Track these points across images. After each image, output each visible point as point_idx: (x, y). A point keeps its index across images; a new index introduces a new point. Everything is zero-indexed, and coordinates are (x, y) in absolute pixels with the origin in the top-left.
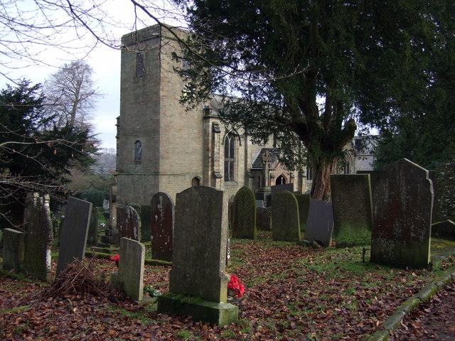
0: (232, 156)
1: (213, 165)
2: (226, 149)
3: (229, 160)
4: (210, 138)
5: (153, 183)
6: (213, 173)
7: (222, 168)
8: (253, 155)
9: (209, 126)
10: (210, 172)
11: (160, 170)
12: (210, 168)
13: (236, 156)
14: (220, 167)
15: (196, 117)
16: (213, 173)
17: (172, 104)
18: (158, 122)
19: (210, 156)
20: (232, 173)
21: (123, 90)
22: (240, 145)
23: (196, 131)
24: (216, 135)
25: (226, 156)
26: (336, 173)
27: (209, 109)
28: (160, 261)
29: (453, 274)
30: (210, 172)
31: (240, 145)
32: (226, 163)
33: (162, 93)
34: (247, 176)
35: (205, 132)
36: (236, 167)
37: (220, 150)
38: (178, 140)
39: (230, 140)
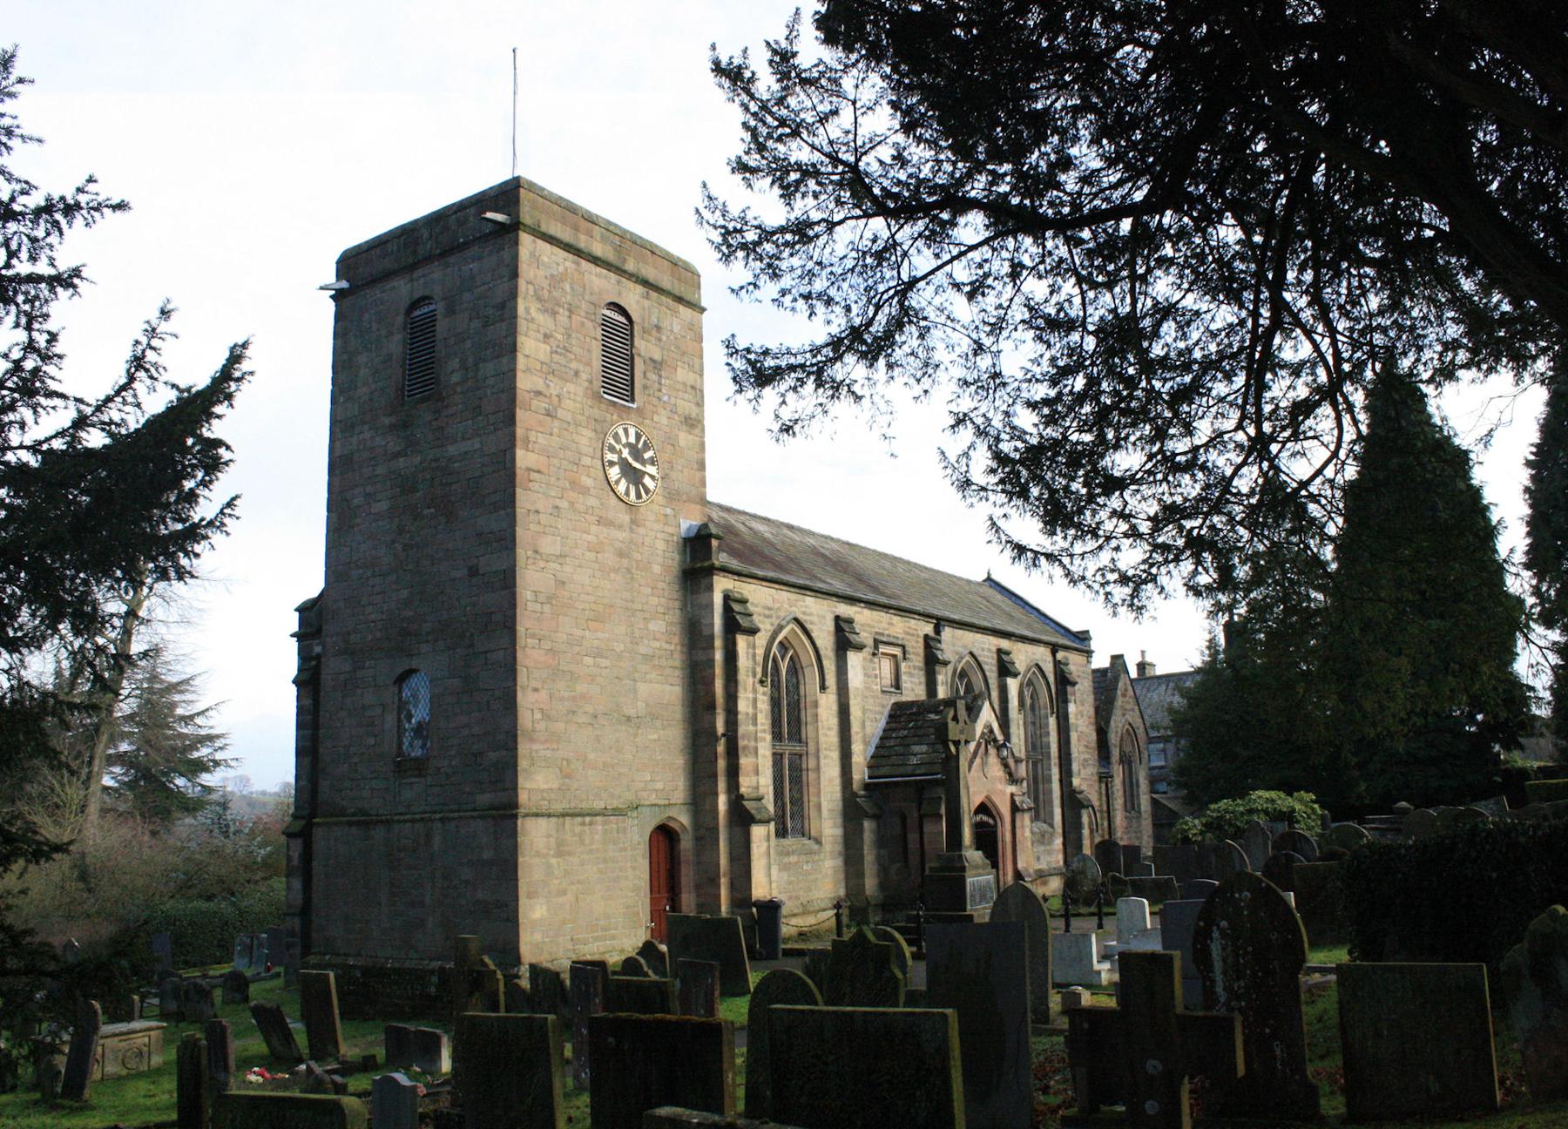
0: (796, 734)
1: (733, 772)
2: (775, 703)
3: (788, 748)
4: (719, 656)
5: (487, 855)
6: (736, 801)
7: (765, 782)
8: (869, 730)
9: (711, 605)
10: (722, 801)
11: (523, 797)
12: (722, 785)
13: (808, 731)
14: (758, 777)
15: (657, 569)
16: (736, 801)
17: (564, 504)
18: (508, 580)
19: (720, 728)
20: (798, 802)
21: (339, 465)
22: (823, 687)
23: (658, 626)
24: (742, 642)
25: (777, 736)
26: (1062, 1039)
27: (710, 536)
28: (721, 764)
29: (1490, 418)
30: (722, 801)
31: (823, 687)
32: (777, 759)
33: (523, 458)
34: (852, 811)
35: (694, 635)
36: (812, 775)
37: (754, 703)
38: (589, 660)
39: (784, 667)
